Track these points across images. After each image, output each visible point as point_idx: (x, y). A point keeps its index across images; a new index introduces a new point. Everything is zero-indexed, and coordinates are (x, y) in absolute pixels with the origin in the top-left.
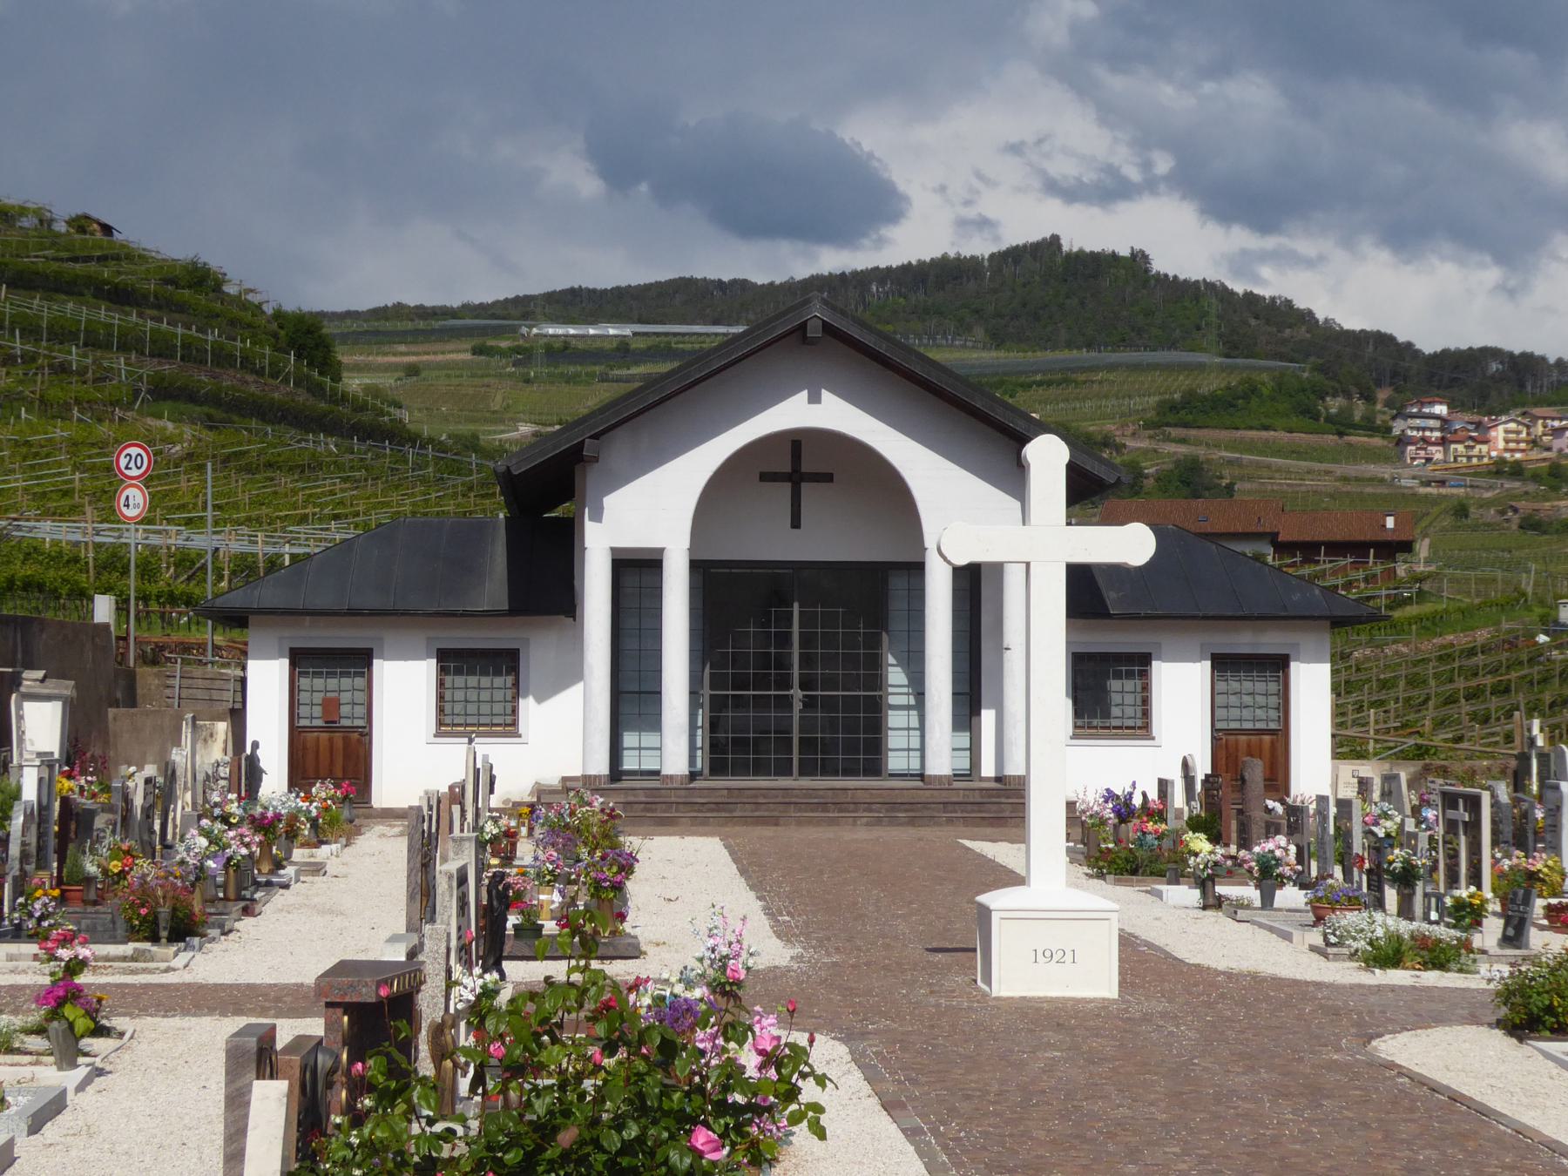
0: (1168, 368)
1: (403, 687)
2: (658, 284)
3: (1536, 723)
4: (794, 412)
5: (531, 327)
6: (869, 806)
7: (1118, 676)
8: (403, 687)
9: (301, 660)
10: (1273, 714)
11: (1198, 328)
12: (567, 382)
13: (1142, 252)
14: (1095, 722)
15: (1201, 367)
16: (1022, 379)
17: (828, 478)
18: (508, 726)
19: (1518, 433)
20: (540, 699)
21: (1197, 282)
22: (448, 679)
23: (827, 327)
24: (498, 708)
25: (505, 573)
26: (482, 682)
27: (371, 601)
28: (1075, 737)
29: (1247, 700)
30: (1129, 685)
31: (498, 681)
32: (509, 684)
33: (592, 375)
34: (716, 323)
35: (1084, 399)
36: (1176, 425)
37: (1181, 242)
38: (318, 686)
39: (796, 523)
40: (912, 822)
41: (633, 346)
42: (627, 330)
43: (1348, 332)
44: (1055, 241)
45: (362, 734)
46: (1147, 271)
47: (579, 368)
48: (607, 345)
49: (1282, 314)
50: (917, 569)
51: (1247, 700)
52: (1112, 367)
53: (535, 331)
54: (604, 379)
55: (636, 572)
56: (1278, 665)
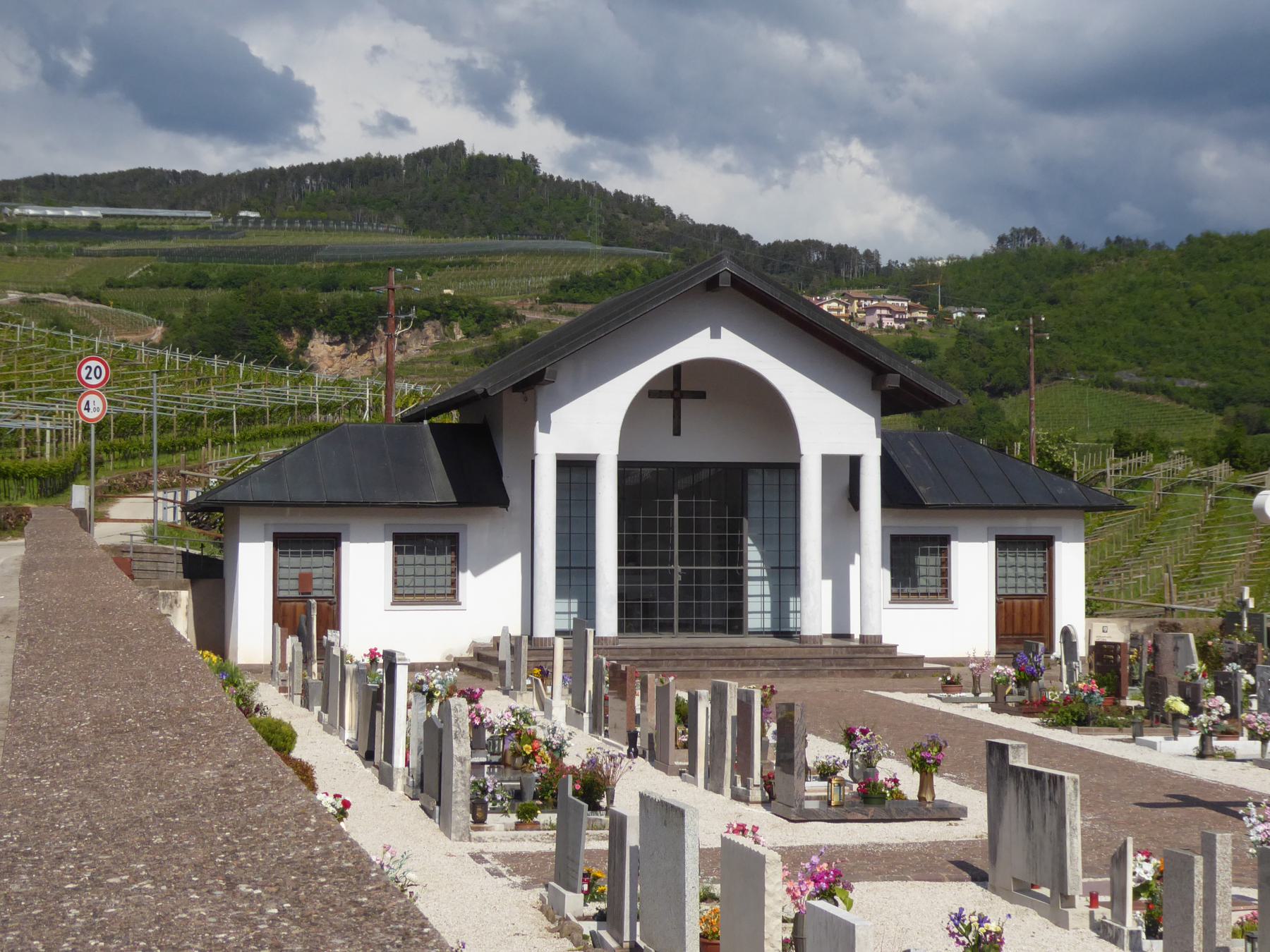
0: (558, 253)
1: (366, 564)
2: (121, 173)
3: (1247, 590)
4: (699, 346)
5: (13, 208)
6: (765, 662)
7: (924, 553)
8: (366, 564)
9: (283, 543)
10: (1040, 582)
11: (578, 220)
12: (47, 256)
13: (532, 156)
14: (906, 590)
15: (585, 254)
16: (438, 260)
17: (701, 395)
18: (450, 595)
19: (839, 310)
20: (476, 573)
21: (577, 182)
22: (400, 557)
23: (736, 282)
24: (440, 581)
25: (457, 471)
26: (430, 562)
27: (342, 495)
28: (892, 602)
29: (1021, 571)
30: (932, 560)
31: (440, 559)
32: (449, 562)
33: (69, 250)
34: (173, 207)
35: (490, 277)
36: (565, 301)
37: (532, 137)
38: (297, 563)
39: (677, 432)
40: (802, 674)
41: (104, 226)
42: (97, 212)
43: (699, 225)
44: (460, 145)
45: (330, 603)
46: (535, 172)
47: (57, 244)
48: (81, 225)
49: (645, 210)
50: (793, 469)
51: (1021, 571)
52: (511, 252)
53: (17, 211)
54: (80, 253)
55: (577, 471)
56: (1045, 544)
